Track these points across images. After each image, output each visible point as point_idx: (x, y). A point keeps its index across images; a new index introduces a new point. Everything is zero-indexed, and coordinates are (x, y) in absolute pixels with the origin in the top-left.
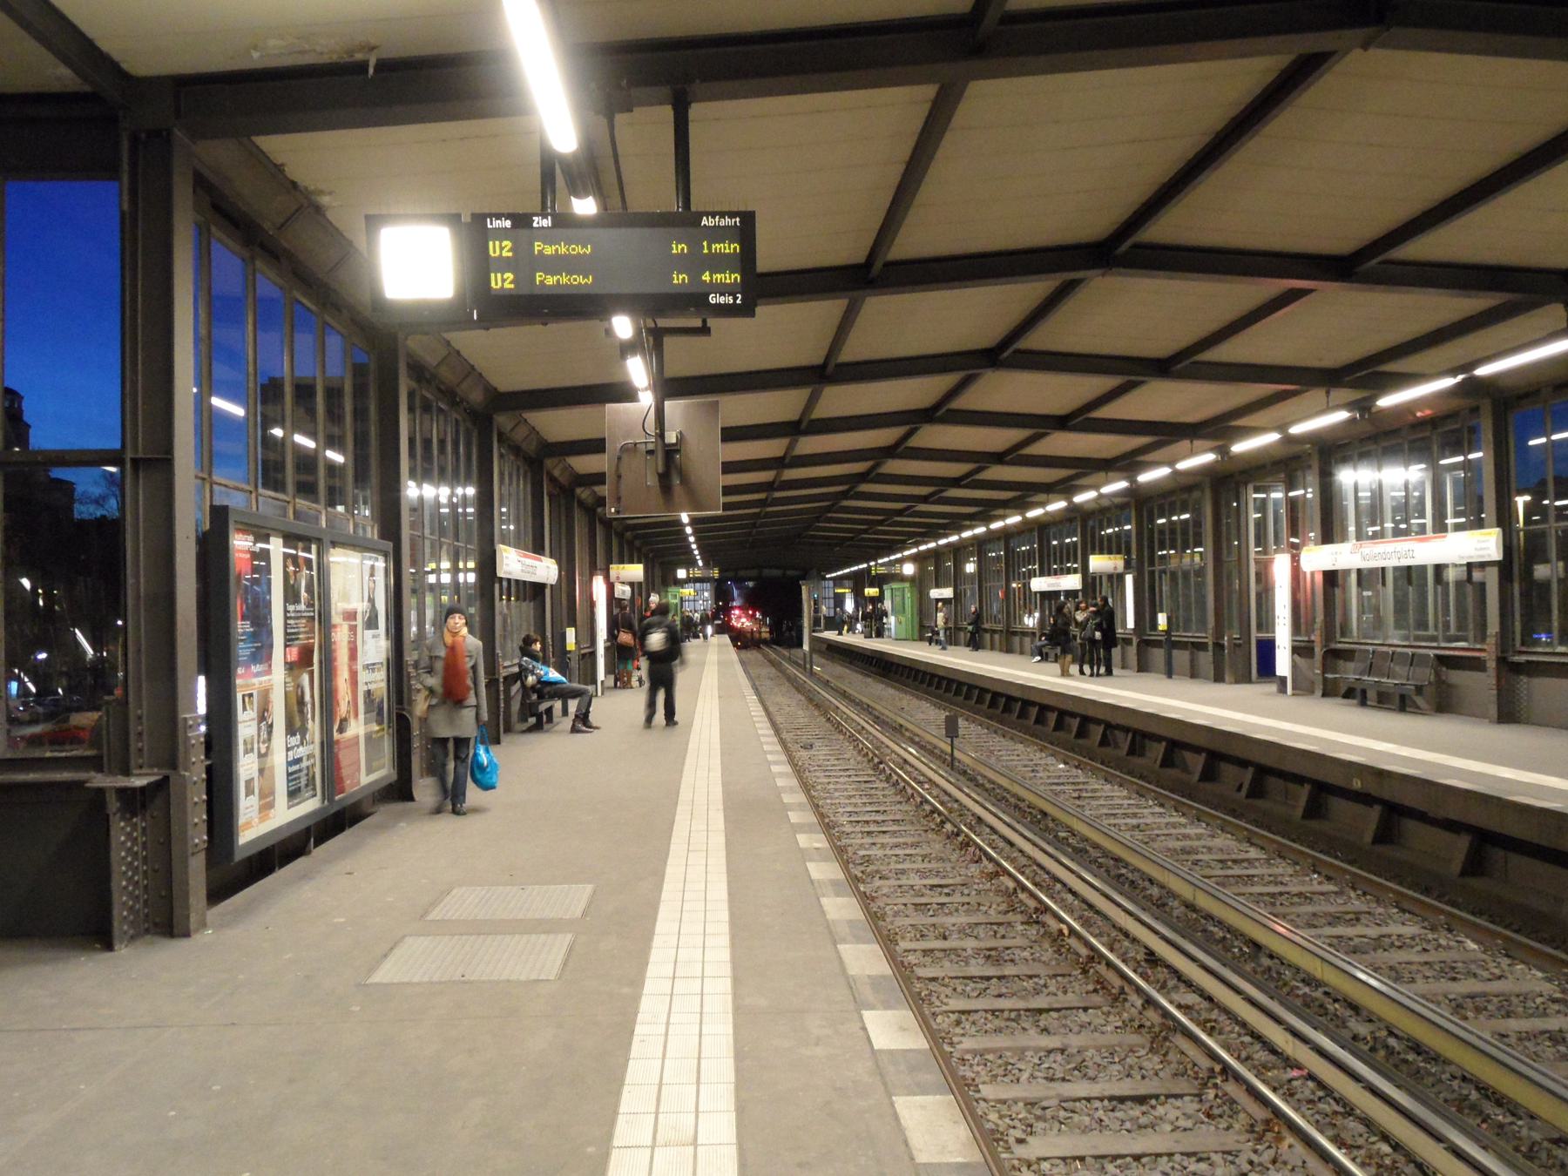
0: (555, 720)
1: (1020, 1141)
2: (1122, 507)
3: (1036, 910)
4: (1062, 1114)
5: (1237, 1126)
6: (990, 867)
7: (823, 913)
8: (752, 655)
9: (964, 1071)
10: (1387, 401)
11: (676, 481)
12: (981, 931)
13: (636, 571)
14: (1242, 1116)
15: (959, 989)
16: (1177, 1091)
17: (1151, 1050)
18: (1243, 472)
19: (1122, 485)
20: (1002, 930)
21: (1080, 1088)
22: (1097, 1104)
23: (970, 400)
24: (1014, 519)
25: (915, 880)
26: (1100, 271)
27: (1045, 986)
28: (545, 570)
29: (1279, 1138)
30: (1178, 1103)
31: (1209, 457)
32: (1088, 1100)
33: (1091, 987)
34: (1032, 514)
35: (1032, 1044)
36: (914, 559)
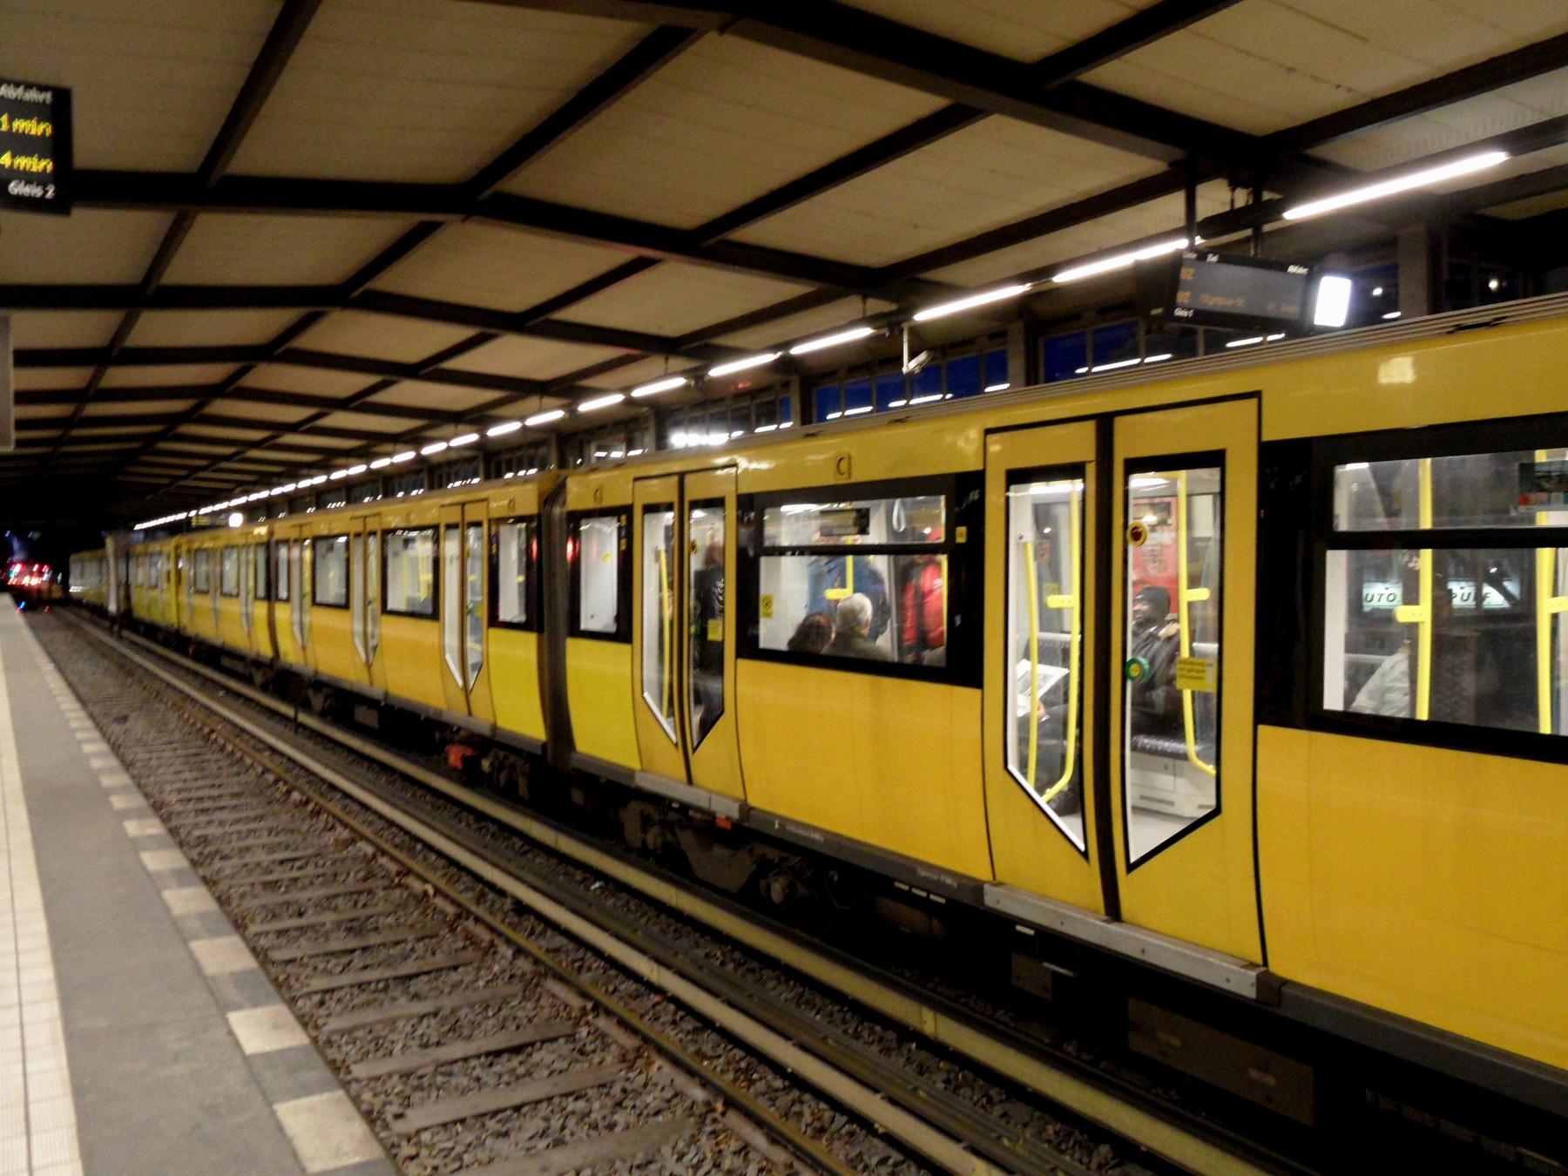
1: (399, 1116)
3: (398, 874)
4: (439, 1079)
5: (609, 1059)
6: (346, 834)
7: (167, 910)
8: (44, 616)
9: (332, 1053)
10: (718, 371)
12: (340, 901)
14: (613, 1047)
15: (321, 967)
16: (552, 1034)
18: (587, 431)
19: (473, 438)
20: (363, 899)
21: (457, 1049)
22: (474, 1062)
23: (309, 340)
24: (358, 469)
25: (263, 858)
26: (462, 216)
27: (413, 950)
29: (649, 1064)
30: (554, 1046)
31: (557, 415)
32: (465, 1060)
33: (460, 944)
34: (377, 464)
35: (404, 1012)
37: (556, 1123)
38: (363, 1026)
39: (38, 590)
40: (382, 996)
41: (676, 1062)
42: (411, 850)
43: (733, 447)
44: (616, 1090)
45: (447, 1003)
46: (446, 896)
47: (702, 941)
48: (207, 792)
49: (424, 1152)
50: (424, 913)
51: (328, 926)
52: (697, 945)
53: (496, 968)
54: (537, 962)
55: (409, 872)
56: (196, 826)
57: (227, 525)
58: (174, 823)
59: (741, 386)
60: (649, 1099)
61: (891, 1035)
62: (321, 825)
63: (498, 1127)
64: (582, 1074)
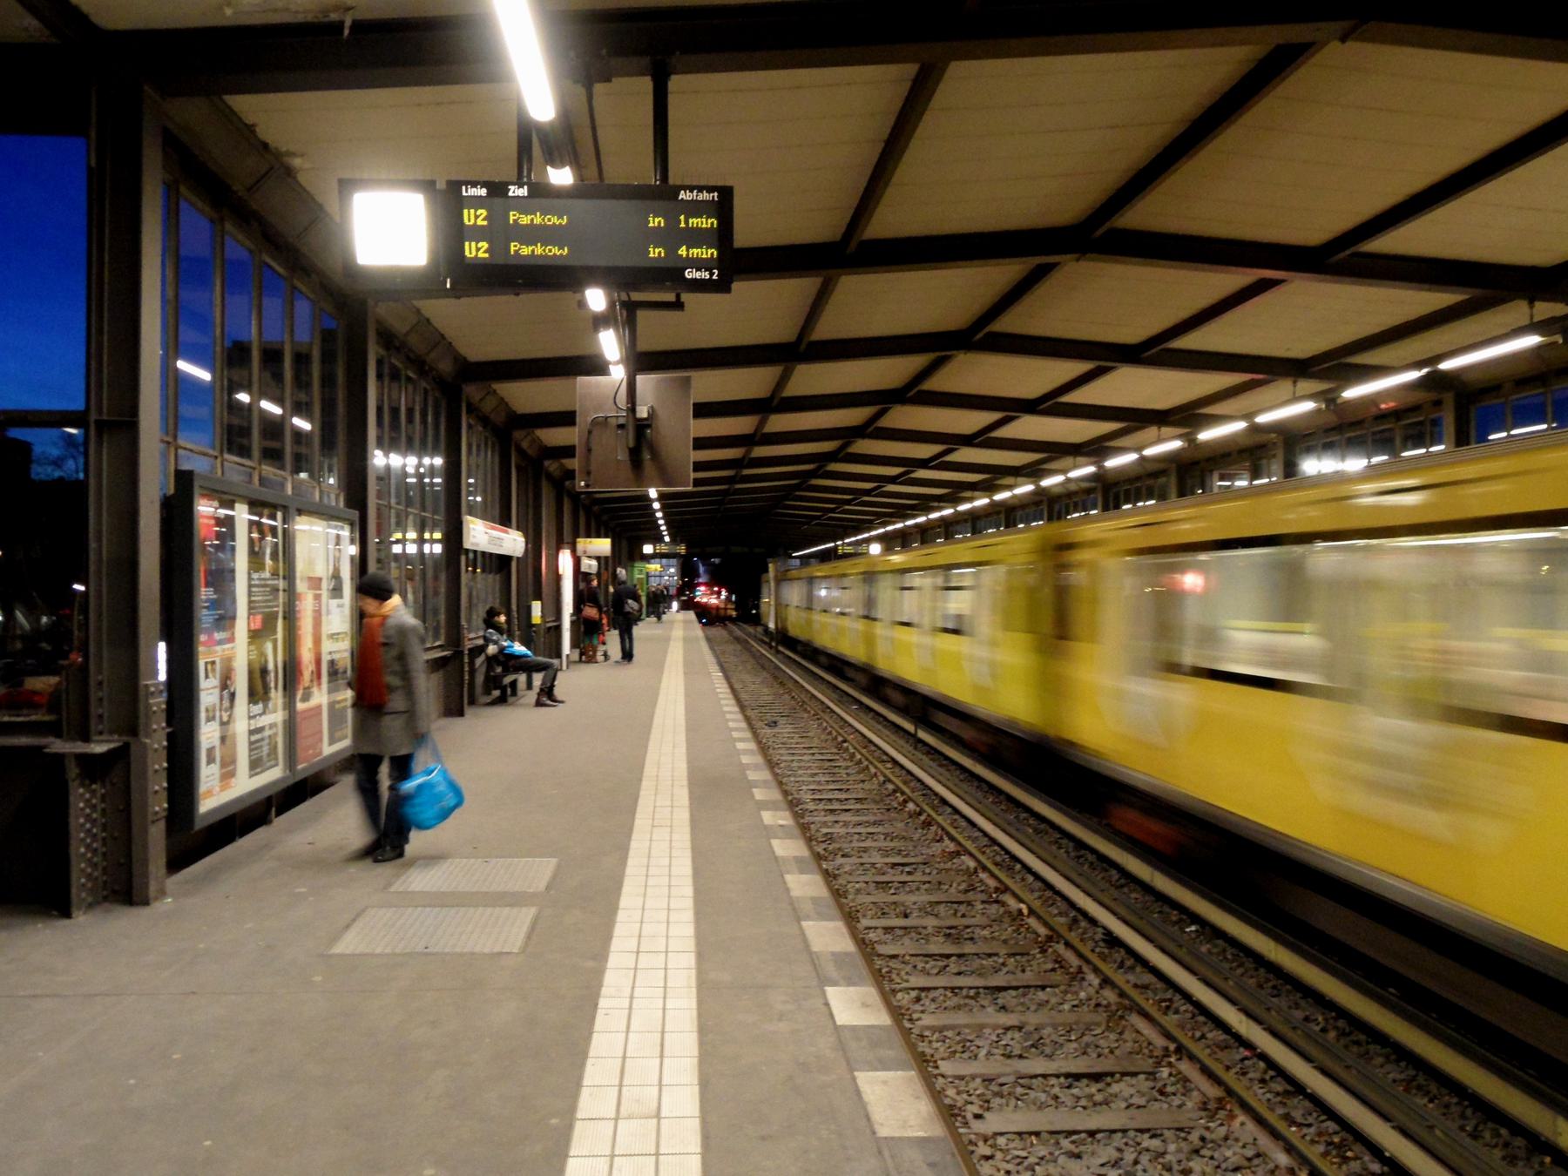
0: (520, 693)
1: (978, 1117)
2: (1088, 491)
3: (997, 890)
4: (1019, 1090)
5: (1190, 1104)
6: (952, 847)
7: (788, 890)
8: (717, 631)
11: (647, 456)
12: (942, 908)
13: (603, 545)
14: (1195, 1093)
16: (1132, 1069)
17: (1108, 1028)
18: (1208, 460)
20: (963, 908)
21: (1037, 1065)
22: (1053, 1081)
23: (942, 382)
25: (878, 859)
28: (512, 542)
29: (1232, 1116)
30: (1133, 1081)
32: (1045, 1076)
33: (1049, 966)
34: (999, 497)
36: (879, 539)
37: (1129, 1156)
38: (952, 1027)
39: (718, 608)
40: (972, 1002)
41: (1260, 1121)
42: (1010, 869)
43: (1372, 473)
44: (1194, 1137)
45: (1033, 1019)
46: (1039, 918)
47: (1303, 1003)
48: (837, 795)
49: (999, 1155)
50: (1017, 931)
51: (930, 930)
52: (1297, 1006)
53: (1083, 995)
54: (1122, 994)
55: (1006, 889)
56: (825, 824)
57: (867, 553)
58: (807, 819)
59: (1383, 406)
60: (1228, 1153)
61: (1519, 1142)
62: (930, 836)
63: (1072, 1147)
64: (1160, 1113)
